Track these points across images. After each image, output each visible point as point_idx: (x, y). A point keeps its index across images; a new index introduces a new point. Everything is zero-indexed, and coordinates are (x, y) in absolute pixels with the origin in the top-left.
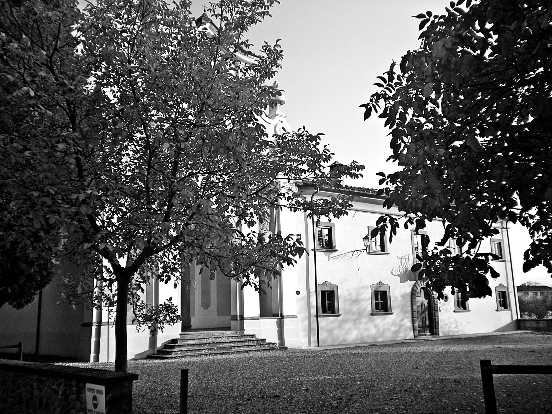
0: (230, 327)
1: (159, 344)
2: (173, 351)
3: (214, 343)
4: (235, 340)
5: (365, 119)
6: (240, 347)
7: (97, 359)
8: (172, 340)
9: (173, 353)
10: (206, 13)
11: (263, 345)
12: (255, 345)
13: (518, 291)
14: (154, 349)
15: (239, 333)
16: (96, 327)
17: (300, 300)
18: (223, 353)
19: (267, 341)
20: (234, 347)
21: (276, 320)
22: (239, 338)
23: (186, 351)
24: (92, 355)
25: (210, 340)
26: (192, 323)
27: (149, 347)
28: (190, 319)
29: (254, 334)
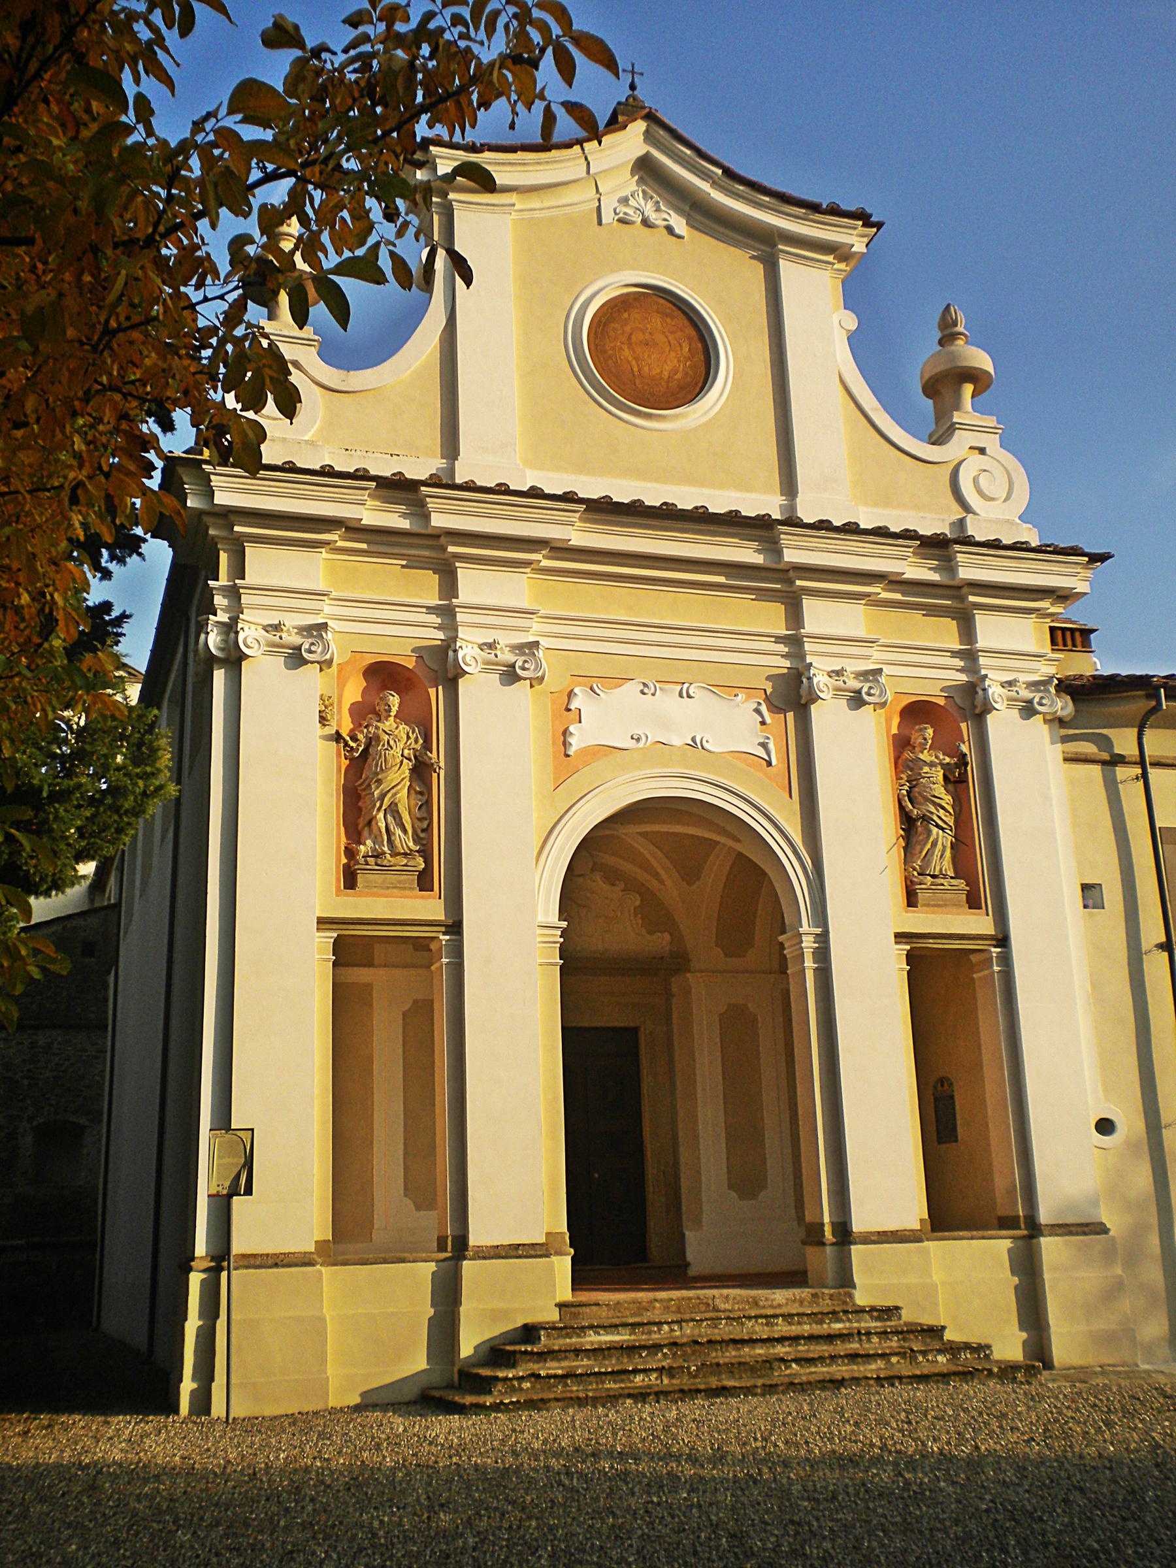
0: (805, 1272)
2: (496, 1378)
3: (696, 1342)
4: (806, 1329)
6: (811, 1361)
7: (202, 1402)
8: (526, 1327)
9: (500, 1386)
11: (924, 1353)
12: (883, 1356)
14: (453, 1365)
15: (831, 1297)
16: (203, 1276)
18: (724, 1388)
19: (948, 1336)
20: (782, 1360)
21: (1008, 1243)
22: (821, 1322)
23: (555, 1376)
24: (187, 1386)
25: (688, 1329)
27: (430, 1358)
28: (684, 1235)
29: (890, 1303)
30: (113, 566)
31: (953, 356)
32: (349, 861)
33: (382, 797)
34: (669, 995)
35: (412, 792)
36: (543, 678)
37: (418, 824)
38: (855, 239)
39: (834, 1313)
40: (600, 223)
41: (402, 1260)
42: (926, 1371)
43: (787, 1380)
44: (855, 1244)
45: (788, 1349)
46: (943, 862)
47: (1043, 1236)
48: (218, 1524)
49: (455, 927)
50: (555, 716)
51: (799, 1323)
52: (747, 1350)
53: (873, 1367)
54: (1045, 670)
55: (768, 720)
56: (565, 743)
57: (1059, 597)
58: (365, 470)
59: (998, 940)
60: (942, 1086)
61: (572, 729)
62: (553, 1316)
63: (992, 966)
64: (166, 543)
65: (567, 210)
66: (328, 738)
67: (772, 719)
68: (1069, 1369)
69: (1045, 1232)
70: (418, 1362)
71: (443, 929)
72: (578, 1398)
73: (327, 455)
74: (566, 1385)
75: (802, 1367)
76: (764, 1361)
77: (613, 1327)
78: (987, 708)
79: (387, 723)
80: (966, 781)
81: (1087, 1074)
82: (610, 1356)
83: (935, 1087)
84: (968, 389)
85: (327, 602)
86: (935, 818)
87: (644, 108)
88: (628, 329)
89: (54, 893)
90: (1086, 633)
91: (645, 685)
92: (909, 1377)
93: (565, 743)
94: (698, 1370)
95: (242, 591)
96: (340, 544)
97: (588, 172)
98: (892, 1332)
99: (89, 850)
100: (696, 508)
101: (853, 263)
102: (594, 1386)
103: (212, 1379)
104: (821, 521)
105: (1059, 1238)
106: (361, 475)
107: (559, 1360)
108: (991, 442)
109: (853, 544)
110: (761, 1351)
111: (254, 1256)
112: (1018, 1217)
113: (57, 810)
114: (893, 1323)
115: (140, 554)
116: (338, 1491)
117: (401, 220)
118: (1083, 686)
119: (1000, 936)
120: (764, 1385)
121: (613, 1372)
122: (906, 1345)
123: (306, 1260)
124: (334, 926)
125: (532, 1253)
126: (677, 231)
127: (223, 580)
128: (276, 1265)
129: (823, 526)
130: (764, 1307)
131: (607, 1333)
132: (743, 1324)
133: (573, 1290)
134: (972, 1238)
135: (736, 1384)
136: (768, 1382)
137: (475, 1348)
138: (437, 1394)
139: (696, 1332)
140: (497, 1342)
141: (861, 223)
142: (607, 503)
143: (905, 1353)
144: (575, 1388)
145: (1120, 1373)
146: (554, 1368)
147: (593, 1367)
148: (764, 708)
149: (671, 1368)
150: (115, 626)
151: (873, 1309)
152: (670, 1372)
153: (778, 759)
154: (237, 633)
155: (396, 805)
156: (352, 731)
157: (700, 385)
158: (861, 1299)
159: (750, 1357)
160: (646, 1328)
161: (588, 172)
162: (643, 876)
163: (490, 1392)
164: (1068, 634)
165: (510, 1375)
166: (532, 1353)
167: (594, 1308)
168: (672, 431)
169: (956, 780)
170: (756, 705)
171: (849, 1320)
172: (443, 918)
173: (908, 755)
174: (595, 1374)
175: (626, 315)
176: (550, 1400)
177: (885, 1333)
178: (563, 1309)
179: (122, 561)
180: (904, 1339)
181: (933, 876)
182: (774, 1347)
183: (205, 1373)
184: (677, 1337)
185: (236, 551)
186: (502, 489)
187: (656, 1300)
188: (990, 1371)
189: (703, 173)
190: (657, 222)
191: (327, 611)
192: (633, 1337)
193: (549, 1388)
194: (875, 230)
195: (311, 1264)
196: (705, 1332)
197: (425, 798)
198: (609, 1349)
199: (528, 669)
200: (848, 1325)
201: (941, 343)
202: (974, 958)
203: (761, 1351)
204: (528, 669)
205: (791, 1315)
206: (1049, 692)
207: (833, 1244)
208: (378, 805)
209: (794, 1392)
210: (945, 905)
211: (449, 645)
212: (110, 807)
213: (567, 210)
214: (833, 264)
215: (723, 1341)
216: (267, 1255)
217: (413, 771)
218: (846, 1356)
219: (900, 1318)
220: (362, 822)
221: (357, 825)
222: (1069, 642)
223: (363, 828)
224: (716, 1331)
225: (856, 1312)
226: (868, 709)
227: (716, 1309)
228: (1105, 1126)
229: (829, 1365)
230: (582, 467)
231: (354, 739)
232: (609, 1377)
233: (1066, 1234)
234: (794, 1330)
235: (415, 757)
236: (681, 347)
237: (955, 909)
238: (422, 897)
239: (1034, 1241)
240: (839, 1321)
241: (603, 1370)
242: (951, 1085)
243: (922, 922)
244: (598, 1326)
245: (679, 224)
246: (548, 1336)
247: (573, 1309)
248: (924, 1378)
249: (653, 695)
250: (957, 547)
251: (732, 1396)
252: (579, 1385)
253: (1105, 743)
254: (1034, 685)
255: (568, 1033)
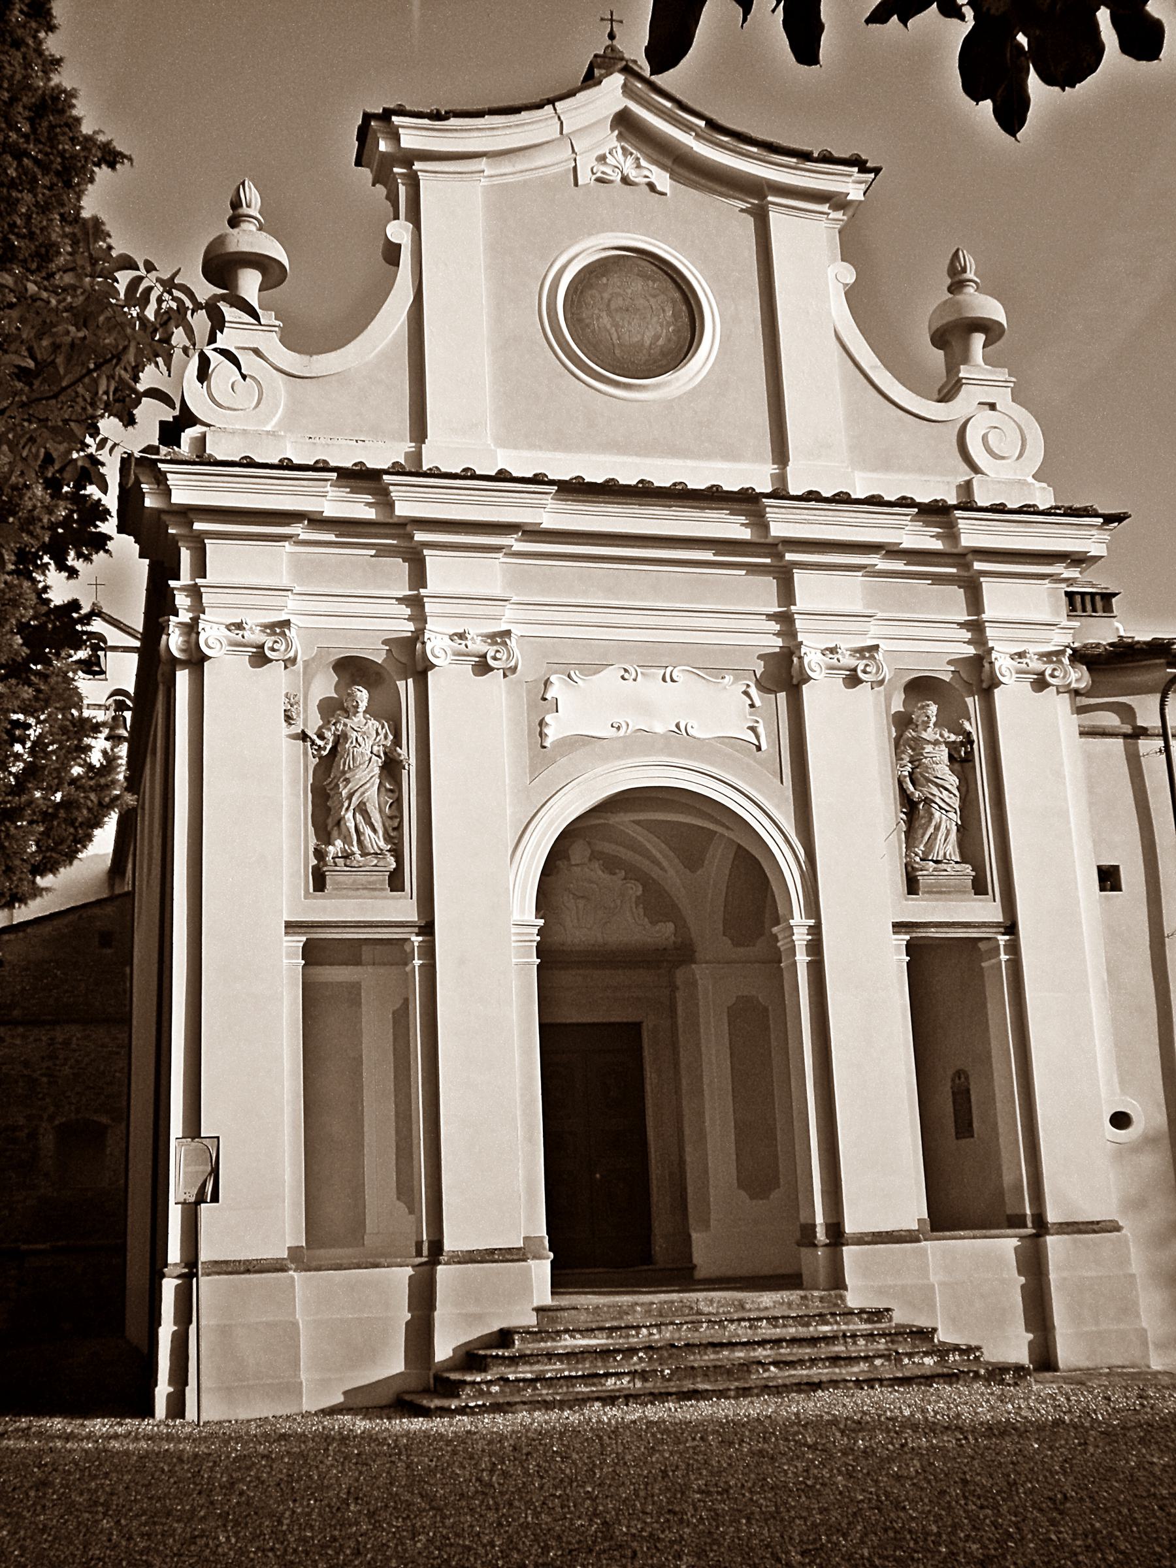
1: (443, 1351)
2: (464, 1382)
3: (673, 1346)
5: (869, 21)
7: (177, 1407)
9: (468, 1390)
10: (615, 42)
11: (910, 1355)
12: (866, 1358)
13: (136, 465)
14: (430, 1369)
15: (822, 1299)
16: (178, 1282)
17: (1136, 1148)
20: (759, 1363)
21: (1015, 1242)
22: (808, 1325)
23: (524, 1380)
24: (163, 1389)
26: (697, 1258)
28: (690, 1236)
29: (881, 1306)
30: (79, 564)
31: (958, 306)
32: (319, 862)
33: (350, 796)
34: (673, 988)
35: (383, 789)
36: (516, 667)
37: (388, 823)
38: (852, 186)
39: (821, 1315)
40: (576, 184)
41: (376, 1266)
42: (908, 1374)
43: (763, 1382)
44: (848, 1245)
45: (769, 1352)
46: (947, 846)
47: (1049, 1234)
48: (144, 1513)
49: (427, 928)
50: (532, 707)
51: (784, 1326)
52: (726, 1353)
53: (856, 1369)
54: (1059, 639)
55: (758, 703)
56: (541, 734)
57: (1073, 561)
58: (325, 462)
59: (1006, 928)
60: (960, 1078)
61: (548, 719)
62: (531, 1320)
63: (999, 954)
64: (132, 539)
65: (541, 173)
66: (295, 737)
67: (761, 698)
68: (1075, 1370)
69: (1052, 1231)
70: (394, 1364)
71: (416, 930)
72: (545, 1401)
73: (289, 445)
74: (535, 1388)
75: (780, 1369)
76: (740, 1364)
77: (588, 1331)
78: (995, 683)
79: (356, 720)
80: (973, 761)
81: (1100, 1065)
82: (584, 1360)
83: (953, 1080)
84: (979, 339)
85: (291, 596)
86: (937, 800)
87: (622, 59)
88: (606, 296)
89: (17, 905)
90: (1107, 597)
91: (626, 670)
92: (890, 1379)
93: (541, 734)
94: (671, 1374)
95: (202, 590)
96: (302, 537)
97: (561, 133)
98: (878, 1334)
99: (45, 864)
100: (675, 484)
101: (850, 212)
102: (565, 1389)
103: (186, 1384)
104: (810, 492)
105: (1066, 1236)
106: (321, 467)
107: (531, 1364)
108: (1003, 398)
109: (845, 514)
110: (741, 1354)
111: (226, 1262)
112: (1025, 1215)
113: (7, 829)
114: (883, 1326)
115: (107, 551)
116: (269, 1486)
117: (100, 437)
118: (1100, 655)
119: (1008, 924)
120: (737, 1388)
121: (583, 1376)
122: (894, 1347)
123: (278, 1266)
124: (303, 930)
125: (508, 1257)
126: (659, 188)
127: (185, 579)
128: (248, 1271)
129: (812, 496)
130: (750, 1310)
131: (584, 1337)
132: (725, 1328)
133: (553, 1293)
134: (974, 1238)
135: (708, 1387)
136: (746, 1385)
137: (454, 1350)
138: (407, 1397)
139: (677, 1336)
140: (472, 1346)
141: (856, 169)
142: (579, 483)
143: (890, 1355)
144: (544, 1392)
145: (1126, 1374)
146: (526, 1372)
147: (563, 1370)
148: (753, 691)
149: (644, 1371)
150: (83, 624)
151: (862, 1311)
152: (644, 1375)
153: (768, 743)
154: (198, 633)
155: (365, 804)
156: (320, 728)
157: (685, 350)
158: (853, 1301)
159: (728, 1359)
160: (624, 1332)
161: (561, 133)
162: (645, 865)
163: (458, 1396)
164: (1088, 599)
165: (478, 1379)
166: (503, 1357)
167: (573, 1312)
168: (654, 401)
169: (961, 760)
170: (744, 688)
171: (837, 1323)
172: (416, 919)
173: (910, 733)
174: (565, 1377)
175: (604, 280)
176: (516, 1403)
177: (872, 1335)
178: (541, 1313)
179: (88, 559)
180: (892, 1342)
181: (937, 862)
182: (754, 1350)
183: (179, 1377)
184: (656, 1341)
185: (196, 548)
186: (468, 474)
187: (637, 1304)
188: (976, 1373)
189: (686, 126)
190: (637, 180)
191: (290, 608)
192: (610, 1341)
193: (519, 1391)
194: (872, 175)
195: (283, 1269)
196: (686, 1334)
197: (396, 795)
198: (582, 1352)
199: (278, 650)
200: (835, 1327)
201: (950, 290)
202: (981, 945)
203: (741, 1354)
204: (278, 650)
205: (776, 1318)
206: (1062, 663)
207: (826, 1245)
208: (346, 804)
209: (769, 1395)
210: (949, 892)
211: (418, 636)
212: (65, 820)
213: (541, 173)
214: (828, 214)
215: (701, 1344)
216: (240, 1261)
217: (383, 768)
218: (827, 1359)
219: (890, 1320)
220: (331, 822)
221: (326, 826)
222: (1089, 607)
223: (332, 829)
224: (696, 1334)
225: (844, 1314)
226: (863, 688)
227: (699, 1313)
228: (1120, 1120)
229: (810, 1368)
230: (560, 443)
231: (321, 736)
232: (579, 1381)
233: (1074, 1233)
234: (778, 1332)
235: (385, 753)
236: (664, 311)
237: (960, 896)
238: (393, 898)
239: (1042, 1239)
240: (827, 1323)
241: (573, 1374)
242: (967, 1078)
243: (923, 910)
244: (573, 1330)
245: (662, 179)
246: (522, 1340)
247: (550, 1314)
248: (906, 1381)
249: (635, 680)
250: (958, 513)
251: (704, 1399)
252: (549, 1388)
253: (1127, 713)
254: (1047, 656)
255: (547, 1030)
